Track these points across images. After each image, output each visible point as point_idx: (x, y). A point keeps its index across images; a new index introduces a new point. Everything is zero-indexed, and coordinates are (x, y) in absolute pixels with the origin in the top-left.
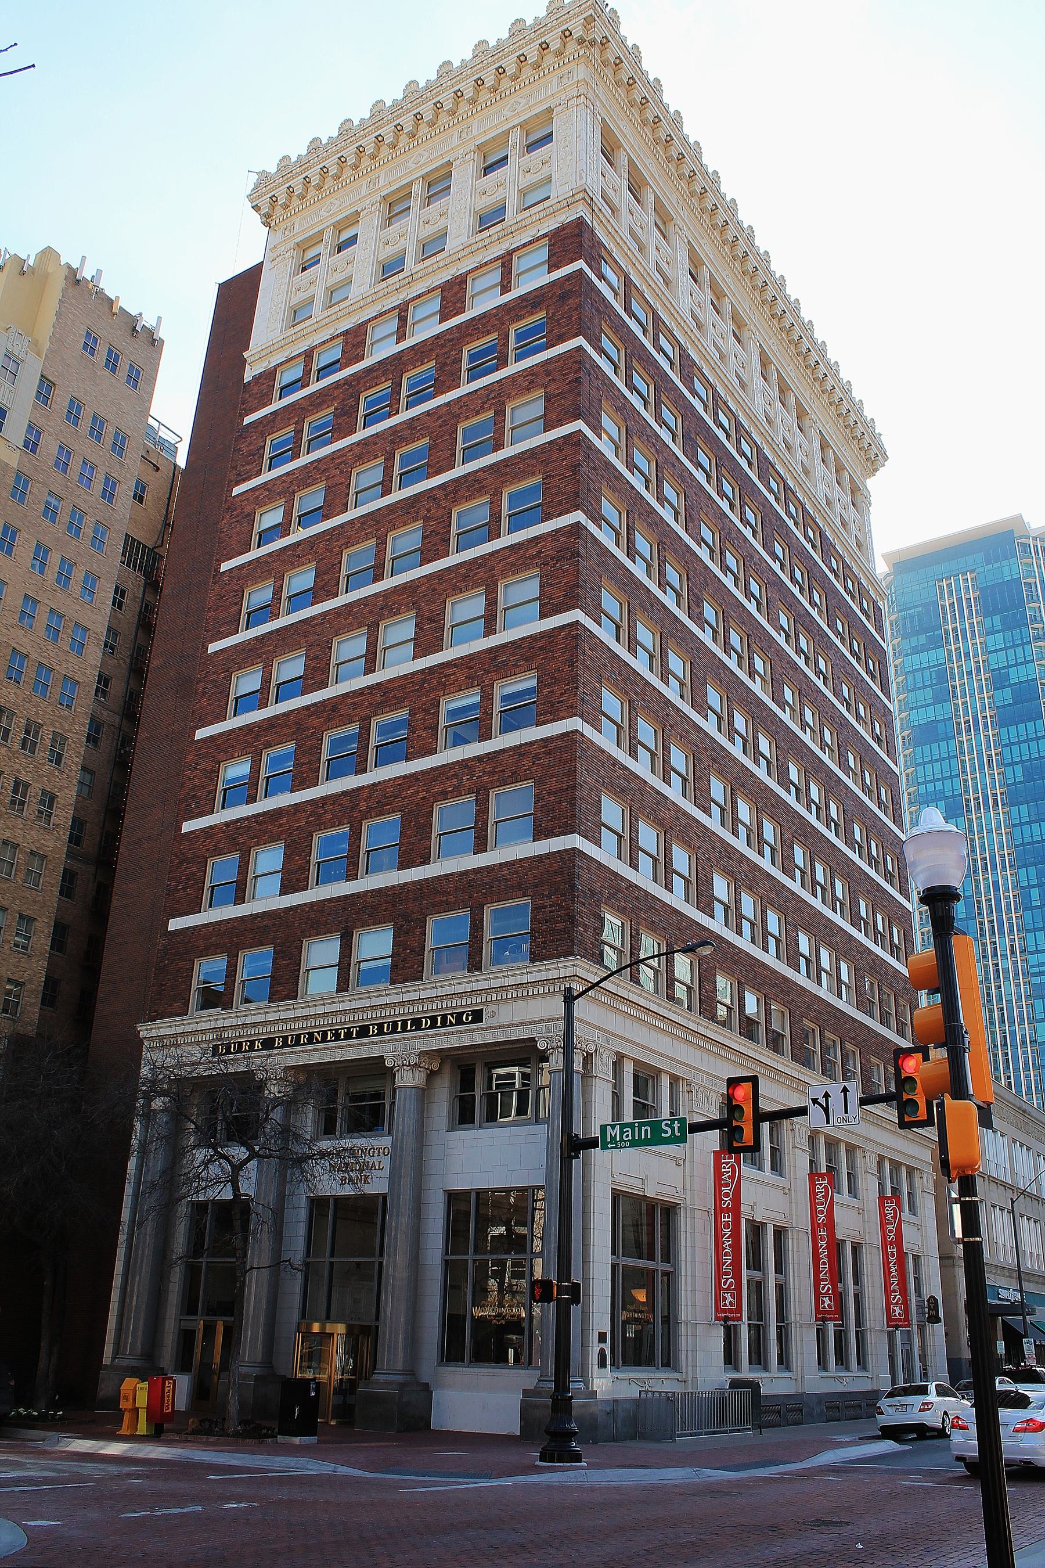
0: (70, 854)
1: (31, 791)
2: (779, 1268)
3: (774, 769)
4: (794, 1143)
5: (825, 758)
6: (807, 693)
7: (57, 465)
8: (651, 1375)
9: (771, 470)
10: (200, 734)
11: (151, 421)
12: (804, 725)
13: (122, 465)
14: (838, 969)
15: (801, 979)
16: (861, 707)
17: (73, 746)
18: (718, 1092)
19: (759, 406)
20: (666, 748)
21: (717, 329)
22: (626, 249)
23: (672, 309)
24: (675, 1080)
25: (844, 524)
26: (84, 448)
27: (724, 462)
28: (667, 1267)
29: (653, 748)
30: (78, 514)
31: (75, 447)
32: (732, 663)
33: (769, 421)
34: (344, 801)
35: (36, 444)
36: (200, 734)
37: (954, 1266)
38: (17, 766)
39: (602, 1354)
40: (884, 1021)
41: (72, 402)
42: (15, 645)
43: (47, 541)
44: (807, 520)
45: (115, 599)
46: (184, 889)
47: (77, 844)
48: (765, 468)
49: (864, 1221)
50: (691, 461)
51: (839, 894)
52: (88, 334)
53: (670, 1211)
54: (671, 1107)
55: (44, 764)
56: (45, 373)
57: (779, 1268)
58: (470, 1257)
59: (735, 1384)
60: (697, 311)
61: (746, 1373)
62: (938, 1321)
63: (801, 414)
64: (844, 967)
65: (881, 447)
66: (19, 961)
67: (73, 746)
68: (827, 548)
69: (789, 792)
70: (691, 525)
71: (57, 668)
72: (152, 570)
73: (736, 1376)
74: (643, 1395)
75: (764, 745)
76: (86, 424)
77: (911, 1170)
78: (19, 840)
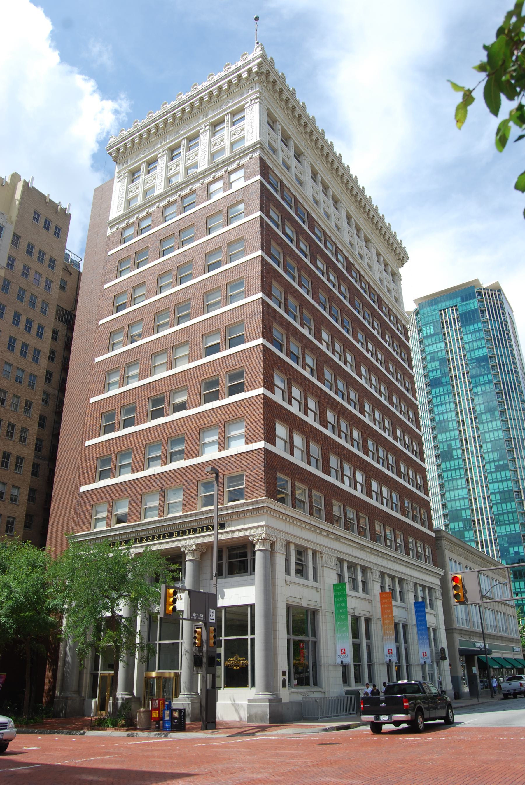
0: (36, 456)
1: (16, 428)
2: (368, 637)
3: (357, 406)
4: (373, 578)
5: (382, 399)
6: (372, 369)
7: (23, 275)
8: (308, 690)
9: (353, 267)
10: (92, 400)
11: (66, 251)
12: (371, 385)
13: (54, 273)
14: (391, 497)
15: (373, 502)
16: (399, 375)
17: (35, 406)
18: (335, 557)
19: (346, 238)
20: (306, 400)
21: (325, 204)
22: (280, 169)
23: (303, 195)
24: (314, 553)
25: (389, 291)
26: (35, 266)
27: (330, 265)
28: (314, 639)
29: (300, 400)
30: (33, 297)
31: (31, 266)
32: (336, 359)
33: (352, 245)
34: (159, 429)
35: (12, 266)
36: (92, 400)
37: (453, 633)
38: (9, 417)
39: (284, 682)
40: (415, 519)
41: (29, 245)
42: (6, 360)
43: (20, 311)
44: (371, 290)
45: (53, 335)
46: (88, 472)
47: (39, 451)
48: (349, 266)
49: (408, 614)
50: (314, 266)
51: (391, 462)
52: (35, 213)
53: (314, 612)
54: (313, 564)
55: (21, 415)
56: (15, 232)
57: (368, 637)
58: (249, 637)
59: (347, 692)
60: (316, 195)
61: (354, 687)
62: (445, 659)
63: (367, 241)
64: (394, 495)
65: (405, 253)
66: (13, 508)
67: (35, 406)
68: (380, 302)
69: (365, 416)
70: (315, 296)
71: (26, 369)
72: (70, 321)
73: (349, 688)
74: (304, 699)
75: (352, 395)
76: (35, 254)
77: (430, 589)
78: (11, 451)
